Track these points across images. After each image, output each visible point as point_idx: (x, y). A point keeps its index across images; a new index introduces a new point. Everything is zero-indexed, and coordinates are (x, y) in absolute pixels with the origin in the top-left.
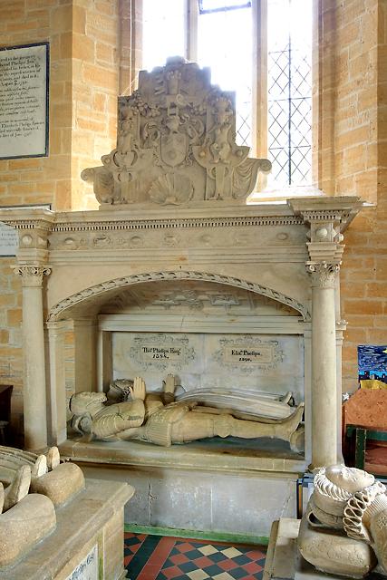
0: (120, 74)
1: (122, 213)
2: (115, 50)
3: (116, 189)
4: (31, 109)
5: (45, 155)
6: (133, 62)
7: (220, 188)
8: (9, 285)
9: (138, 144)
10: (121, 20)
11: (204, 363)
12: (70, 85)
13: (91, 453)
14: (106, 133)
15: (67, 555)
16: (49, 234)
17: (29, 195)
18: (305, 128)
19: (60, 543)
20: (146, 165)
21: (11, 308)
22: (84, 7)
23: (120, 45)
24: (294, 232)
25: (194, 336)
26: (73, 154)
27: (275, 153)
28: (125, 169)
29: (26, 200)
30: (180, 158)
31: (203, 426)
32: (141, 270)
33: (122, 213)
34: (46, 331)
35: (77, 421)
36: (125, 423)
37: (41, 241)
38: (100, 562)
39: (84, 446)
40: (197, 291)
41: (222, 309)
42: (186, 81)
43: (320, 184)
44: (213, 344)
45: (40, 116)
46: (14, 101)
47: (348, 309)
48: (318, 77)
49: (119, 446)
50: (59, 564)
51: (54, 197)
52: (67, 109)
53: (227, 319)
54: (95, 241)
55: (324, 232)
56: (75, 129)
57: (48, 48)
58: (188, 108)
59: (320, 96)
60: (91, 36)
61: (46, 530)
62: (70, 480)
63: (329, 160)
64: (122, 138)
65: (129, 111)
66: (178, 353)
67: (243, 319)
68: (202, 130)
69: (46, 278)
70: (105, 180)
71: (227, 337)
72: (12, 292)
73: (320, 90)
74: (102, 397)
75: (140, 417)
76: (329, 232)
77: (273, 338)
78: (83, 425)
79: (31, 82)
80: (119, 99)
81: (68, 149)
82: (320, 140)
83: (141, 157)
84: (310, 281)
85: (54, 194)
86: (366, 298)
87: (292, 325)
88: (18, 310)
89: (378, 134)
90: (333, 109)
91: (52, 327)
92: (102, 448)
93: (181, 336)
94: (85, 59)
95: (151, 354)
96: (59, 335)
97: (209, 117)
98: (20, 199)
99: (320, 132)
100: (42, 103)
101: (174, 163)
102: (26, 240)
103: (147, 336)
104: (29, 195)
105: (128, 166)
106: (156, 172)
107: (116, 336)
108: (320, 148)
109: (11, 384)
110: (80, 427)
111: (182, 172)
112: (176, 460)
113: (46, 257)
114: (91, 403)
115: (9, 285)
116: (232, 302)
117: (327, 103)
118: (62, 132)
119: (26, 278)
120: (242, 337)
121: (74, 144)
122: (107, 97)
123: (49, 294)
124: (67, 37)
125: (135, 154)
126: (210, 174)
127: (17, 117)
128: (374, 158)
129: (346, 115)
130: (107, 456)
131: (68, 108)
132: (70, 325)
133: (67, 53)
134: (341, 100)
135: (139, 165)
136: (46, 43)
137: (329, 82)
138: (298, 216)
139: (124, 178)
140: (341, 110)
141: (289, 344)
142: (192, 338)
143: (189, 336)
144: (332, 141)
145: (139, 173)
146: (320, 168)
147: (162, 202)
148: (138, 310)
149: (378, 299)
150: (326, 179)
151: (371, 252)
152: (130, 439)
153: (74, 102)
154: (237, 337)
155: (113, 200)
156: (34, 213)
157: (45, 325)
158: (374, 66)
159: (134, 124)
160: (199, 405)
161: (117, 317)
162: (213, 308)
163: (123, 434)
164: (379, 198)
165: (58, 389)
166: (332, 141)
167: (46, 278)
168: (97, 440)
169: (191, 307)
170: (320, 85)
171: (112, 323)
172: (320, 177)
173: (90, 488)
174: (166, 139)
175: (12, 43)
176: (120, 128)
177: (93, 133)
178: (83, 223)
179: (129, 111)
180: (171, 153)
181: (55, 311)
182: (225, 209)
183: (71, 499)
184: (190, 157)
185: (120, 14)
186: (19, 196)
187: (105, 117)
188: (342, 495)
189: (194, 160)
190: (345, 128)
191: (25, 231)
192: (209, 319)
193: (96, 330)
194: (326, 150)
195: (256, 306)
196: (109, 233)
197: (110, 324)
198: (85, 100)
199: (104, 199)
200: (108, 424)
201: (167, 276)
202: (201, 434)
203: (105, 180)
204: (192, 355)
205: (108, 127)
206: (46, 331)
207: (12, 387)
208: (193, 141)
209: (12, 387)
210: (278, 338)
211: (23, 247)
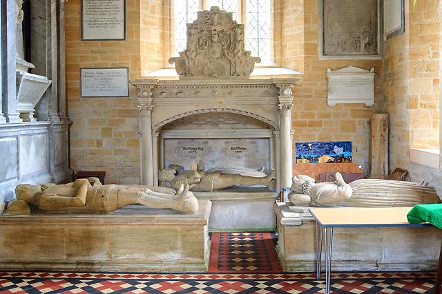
4: (114, 12)
5: (124, 39)
7: (238, 71)
8: (102, 113)
11: (217, 155)
14: (156, 27)
18: (266, 28)
20: (201, 58)
21: (103, 127)
24: (271, 91)
25: (261, 140)
26: (141, 40)
27: (251, 41)
28: (192, 59)
29: (112, 64)
30: (218, 55)
31: (229, 182)
32: (201, 107)
40: (213, 118)
41: (228, 125)
42: (221, 19)
43: (275, 60)
44: (221, 144)
45: (120, 17)
46: (103, 7)
47: (294, 125)
48: (273, 3)
52: (138, 14)
53: (232, 130)
54: (177, 94)
55: (286, 92)
56: (142, 25)
58: (222, 31)
59: (275, 13)
63: (280, 48)
65: (193, 31)
66: (202, 149)
67: (238, 130)
68: (229, 42)
71: (230, 140)
72: (104, 117)
73: (275, 10)
76: (288, 92)
77: (254, 140)
80: (187, 24)
81: (138, 36)
82: (275, 36)
84: (279, 112)
85: (130, 62)
86: (299, 119)
87: (266, 133)
88: (108, 129)
89: (305, 38)
90: (282, 20)
93: (204, 141)
95: (187, 151)
97: (232, 37)
98: (108, 64)
99: (275, 32)
101: (215, 57)
103: (185, 141)
104: (114, 62)
106: (206, 61)
108: (275, 41)
109: (104, 170)
111: (219, 61)
112: (218, 197)
115: (102, 113)
116: (235, 122)
117: (278, 18)
118: (134, 28)
120: (237, 140)
122: (157, 6)
126: (233, 63)
128: (303, 50)
129: (288, 26)
131: (138, 13)
134: (286, 17)
135: (200, 57)
137: (279, 7)
138: (274, 85)
139: (191, 64)
140: (285, 23)
141: (261, 143)
142: (210, 141)
143: (209, 141)
144: (281, 37)
146: (275, 51)
147: (211, 75)
148: (183, 127)
149: (305, 120)
150: (278, 57)
151: (301, 97)
154: (234, 140)
155: (185, 74)
158: (303, 5)
159: (195, 38)
160: (222, 174)
161: (172, 131)
162: (225, 125)
164: (305, 70)
166: (281, 37)
169: (212, 125)
170: (275, 7)
172: (275, 56)
174: (211, 46)
176: (188, 39)
180: (214, 53)
182: (240, 81)
184: (223, 54)
186: (107, 62)
187: (156, 18)
188: (302, 182)
189: (225, 56)
190: (288, 32)
192: (223, 130)
194: (278, 42)
195: (247, 123)
197: (167, 135)
198: (146, 9)
201: (213, 110)
202: (227, 185)
204: (210, 151)
205: (157, 23)
207: (105, 172)
208: (225, 47)
210: (256, 140)
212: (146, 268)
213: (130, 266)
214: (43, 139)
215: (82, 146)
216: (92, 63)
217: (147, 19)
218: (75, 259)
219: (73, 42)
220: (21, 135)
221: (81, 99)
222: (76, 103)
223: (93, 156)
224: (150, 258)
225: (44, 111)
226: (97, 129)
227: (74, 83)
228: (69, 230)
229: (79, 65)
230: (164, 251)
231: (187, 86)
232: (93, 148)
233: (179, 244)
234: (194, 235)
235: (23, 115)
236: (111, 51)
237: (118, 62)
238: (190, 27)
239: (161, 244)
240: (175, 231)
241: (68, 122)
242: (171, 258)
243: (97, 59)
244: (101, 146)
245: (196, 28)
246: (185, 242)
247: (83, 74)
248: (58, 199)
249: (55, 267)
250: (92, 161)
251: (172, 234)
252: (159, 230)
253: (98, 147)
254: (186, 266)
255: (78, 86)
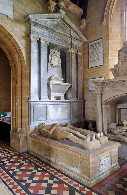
0: (122, 41)
1: (119, 79)
2: (120, 35)
3: (118, 73)
6: (126, 37)
9: (123, 61)
10: (122, 27)
12: (108, 47)
13: (114, 137)
15: (102, 152)
16: (102, 85)
17: (99, 75)
19: (100, 149)
22: (26, 98)
23: (122, 33)
26: (110, 64)
29: (99, 76)
33: (119, 79)
34: (102, 107)
35: (110, 129)
36: (121, 130)
37: (100, 87)
38: (111, 158)
39: (111, 135)
45: (101, 56)
49: (120, 136)
50: (100, 153)
51: (105, 75)
52: (108, 53)
56: (110, 57)
57: (103, 39)
60: (114, 33)
61: (98, 146)
62: (105, 139)
64: (119, 60)
69: (102, 95)
70: (115, 71)
74: (116, 124)
75: (125, 129)
78: (111, 131)
79: (99, 48)
81: (108, 63)
83: (124, 64)
91: (103, 106)
92: (116, 136)
94: (112, 39)
96: (105, 108)
100: (102, 53)
102: (97, 87)
104: (99, 75)
105: (121, 67)
107: (121, 109)
110: (110, 131)
113: (102, 90)
114: (114, 125)
119: (97, 95)
121: (110, 61)
123: (102, 99)
124: (108, 35)
125: (122, 64)
127: (96, 57)
130: (116, 138)
131: (108, 53)
132: (109, 106)
133: (108, 39)
135: (124, 66)
136: (103, 38)
139: (120, 70)
145: (124, 68)
152: (123, 135)
153: (109, 51)
156: (98, 80)
157: (102, 106)
159: (122, 57)
161: (123, 105)
163: (121, 133)
165: (105, 121)
167: (102, 95)
168: (114, 134)
171: (120, 106)
173: (110, 142)
175: (95, 40)
176: (119, 58)
177: (115, 58)
178: (110, 81)
179: (121, 53)
181: (104, 103)
183: (105, 143)
185: (122, 25)
191: (97, 85)
193: (116, 108)
196: (116, 84)
198: (112, 50)
199: (115, 75)
200: (117, 131)
203: (115, 71)
206: (102, 107)
207: (96, 121)
209: (96, 121)
211: (96, 88)
212: (66, 172)
213: (61, 168)
214: (67, 106)
215: (88, 110)
216: (92, 77)
217: (113, 54)
218: (46, 157)
219: (86, 69)
220: (49, 105)
221: (88, 91)
222: (87, 93)
223: (92, 114)
224: (68, 168)
225: (69, 95)
226: (93, 103)
227: (86, 85)
228: (45, 144)
229: (87, 78)
230: (73, 167)
231: (118, 82)
232: (92, 111)
233: (79, 166)
234: (86, 163)
235: (58, 98)
236: (98, 71)
237: (101, 75)
238: (119, 51)
239: (72, 162)
240: (77, 157)
241: (84, 100)
242: (76, 171)
243: (93, 75)
244: (95, 110)
245: (122, 51)
246: (82, 166)
247: (89, 81)
248: (45, 131)
249: (41, 158)
250: (92, 116)
251: (76, 158)
252: (72, 155)
253: (94, 110)
254: (82, 179)
255: (87, 86)
